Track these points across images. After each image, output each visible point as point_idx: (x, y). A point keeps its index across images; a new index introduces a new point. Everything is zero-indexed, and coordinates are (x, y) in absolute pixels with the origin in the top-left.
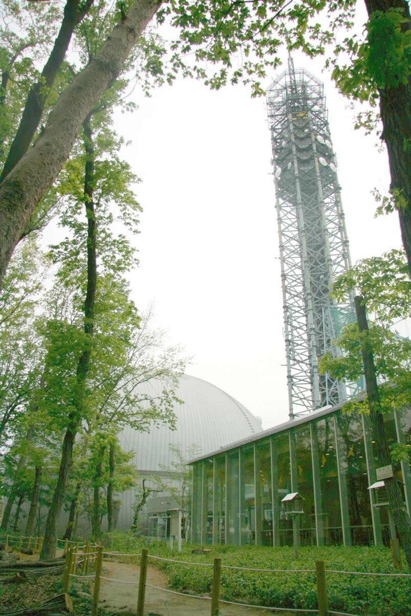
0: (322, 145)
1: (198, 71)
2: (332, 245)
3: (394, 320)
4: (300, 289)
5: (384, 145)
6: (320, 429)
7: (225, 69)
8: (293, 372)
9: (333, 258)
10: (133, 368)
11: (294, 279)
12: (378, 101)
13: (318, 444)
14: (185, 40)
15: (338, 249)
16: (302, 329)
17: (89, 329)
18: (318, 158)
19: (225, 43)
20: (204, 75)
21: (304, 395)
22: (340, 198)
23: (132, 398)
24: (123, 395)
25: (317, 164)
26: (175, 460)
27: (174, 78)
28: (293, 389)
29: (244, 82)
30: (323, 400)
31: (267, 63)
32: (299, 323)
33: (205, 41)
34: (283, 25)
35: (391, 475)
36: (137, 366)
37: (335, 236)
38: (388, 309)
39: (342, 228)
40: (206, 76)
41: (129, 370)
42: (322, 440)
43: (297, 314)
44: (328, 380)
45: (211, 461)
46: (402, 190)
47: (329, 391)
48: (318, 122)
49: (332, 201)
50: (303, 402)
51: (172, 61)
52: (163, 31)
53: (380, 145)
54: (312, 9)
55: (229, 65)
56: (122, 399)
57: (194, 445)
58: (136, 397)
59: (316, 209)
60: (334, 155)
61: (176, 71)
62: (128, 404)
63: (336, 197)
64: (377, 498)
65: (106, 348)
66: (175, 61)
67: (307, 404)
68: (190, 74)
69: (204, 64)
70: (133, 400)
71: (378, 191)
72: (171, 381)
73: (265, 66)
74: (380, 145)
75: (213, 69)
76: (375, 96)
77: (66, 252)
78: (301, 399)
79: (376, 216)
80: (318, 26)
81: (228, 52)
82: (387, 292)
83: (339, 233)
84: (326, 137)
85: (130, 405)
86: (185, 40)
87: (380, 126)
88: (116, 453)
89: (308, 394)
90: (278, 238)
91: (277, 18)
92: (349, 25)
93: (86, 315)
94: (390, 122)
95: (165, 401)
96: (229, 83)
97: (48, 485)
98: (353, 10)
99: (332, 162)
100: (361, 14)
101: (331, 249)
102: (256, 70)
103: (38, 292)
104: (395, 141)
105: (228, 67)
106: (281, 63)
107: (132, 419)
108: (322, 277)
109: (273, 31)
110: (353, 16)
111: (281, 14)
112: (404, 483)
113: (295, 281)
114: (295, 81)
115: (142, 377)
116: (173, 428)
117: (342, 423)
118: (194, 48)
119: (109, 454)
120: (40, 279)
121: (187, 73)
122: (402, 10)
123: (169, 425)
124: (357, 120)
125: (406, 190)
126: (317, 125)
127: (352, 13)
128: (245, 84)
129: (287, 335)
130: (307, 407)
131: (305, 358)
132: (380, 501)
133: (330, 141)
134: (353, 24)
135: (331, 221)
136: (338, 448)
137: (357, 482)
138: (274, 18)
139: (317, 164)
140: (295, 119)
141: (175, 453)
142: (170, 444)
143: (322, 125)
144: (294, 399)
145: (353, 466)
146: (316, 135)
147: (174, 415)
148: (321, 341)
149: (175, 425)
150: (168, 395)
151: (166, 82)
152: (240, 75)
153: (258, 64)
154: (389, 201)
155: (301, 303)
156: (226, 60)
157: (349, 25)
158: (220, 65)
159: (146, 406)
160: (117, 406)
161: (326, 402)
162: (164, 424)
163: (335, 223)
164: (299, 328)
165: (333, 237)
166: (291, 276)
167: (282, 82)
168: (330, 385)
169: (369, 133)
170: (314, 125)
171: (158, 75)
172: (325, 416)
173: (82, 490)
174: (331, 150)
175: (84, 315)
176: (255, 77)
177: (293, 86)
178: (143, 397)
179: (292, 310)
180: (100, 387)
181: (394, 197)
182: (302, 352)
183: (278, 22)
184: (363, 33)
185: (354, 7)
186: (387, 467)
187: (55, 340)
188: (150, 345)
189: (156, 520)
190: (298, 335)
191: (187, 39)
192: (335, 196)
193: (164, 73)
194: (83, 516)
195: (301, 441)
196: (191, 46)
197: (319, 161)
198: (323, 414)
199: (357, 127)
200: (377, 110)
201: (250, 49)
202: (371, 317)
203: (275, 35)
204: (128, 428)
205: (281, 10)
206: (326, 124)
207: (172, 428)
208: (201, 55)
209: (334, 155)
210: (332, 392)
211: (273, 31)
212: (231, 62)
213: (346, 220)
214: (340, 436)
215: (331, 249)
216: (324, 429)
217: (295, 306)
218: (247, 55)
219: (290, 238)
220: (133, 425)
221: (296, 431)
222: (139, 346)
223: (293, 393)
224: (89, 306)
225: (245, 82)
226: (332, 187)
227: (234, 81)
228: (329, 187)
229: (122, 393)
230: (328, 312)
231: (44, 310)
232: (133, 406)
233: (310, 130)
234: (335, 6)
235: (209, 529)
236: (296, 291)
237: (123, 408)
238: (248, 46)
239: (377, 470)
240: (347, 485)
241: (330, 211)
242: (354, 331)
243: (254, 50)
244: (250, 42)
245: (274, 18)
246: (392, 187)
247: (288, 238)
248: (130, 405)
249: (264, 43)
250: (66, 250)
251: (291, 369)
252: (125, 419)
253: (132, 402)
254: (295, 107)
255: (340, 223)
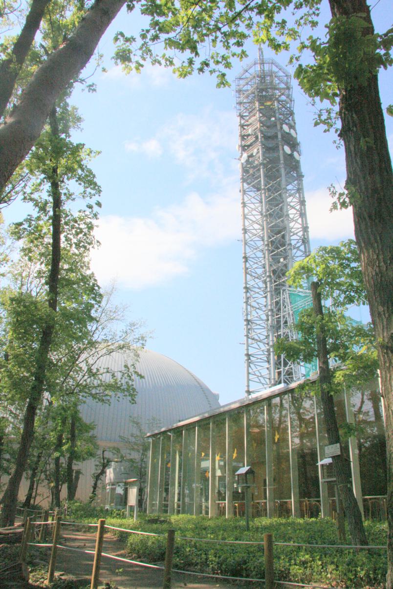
0: (287, 133)
1: (167, 60)
2: (293, 230)
3: (348, 306)
4: (260, 271)
5: (342, 142)
6: (274, 406)
7: (193, 58)
8: (251, 351)
9: (293, 243)
10: (96, 342)
11: (255, 261)
12: (337, 99)
13: (271, 421)
14: (154, 29)
15: (298, 234)
16: (261, 310)
17: (53, 303)
18: (283, 146)
19: (194, 32)
20: (171, 63)
21: (260, 373)
22: (302, 185)
23: (95, 371)
24: (85, 368)
25: (281, 152)
26: (134, 432)
27: (142, 66)
28: (250, 366)
29: (210, 71)
30: (278, 378)
31: (234, 55)
32: (258, 303)
33: (175, 31)
34: (250, 19)
35: (339, 453)
36: (99, 340)
37: (296, 222)
38: (343, 296)
39: (303, 215)
40: (174, 65)
41: (92, 344)
42: (276, 416)
43: (257, 295)
44: (284, 360)
45: (170, 434)
46: (357, 187)
47: (284, 370)
48: (284, 112)
49: (295, 188)
50: (259, 380)
51: (141, 49)
52: (129, 21)
53: (338, 142)
54: (279, 4)
55: (197, 54)
56: (84, 372)
57: (154, 419)
58: (98, 370)
59: (279, 195)
60: (298, 144)
61: (144, 59)
62: (90, 377)
63: (299, 184)
64: (325, 474)
65: (69, 321)
66: (144, 49)
67: (263, 381)
68: (159, 63)
69: (172, 52)
70: (96, 373)
71: (334, 187)
72: (132, 354)
73: (231, 57)
74: (338, 142)
75: (181, 57)
76: (335, 95)
77: (30, 229)
78: (258, 376)
79: (331, 210)
80: (284, 22)
81: (196, 42)
82: (343, 279)
83: (300, 219)
84: (292, 127)
85: (92, 378)
86: (154, 29)
87: (339, 124)
88: (77, 424)
89: (265, 372)
90: (242, 221)
91: (245, 12)
92: (314, 24)
93: (50, 289)
94: (349, 122)
95: (126, 375)
96: (196, 72)
97: (10, 454)
98: (318, 9)
99: (296, 151)
100: (325, 13)
101: (292, 234)
102: (222, 60)
103: (5, 264)
104: (353, 139)
105: (196, 56)
106: (246, 56)
107: (94, 392)
108: (282, 260)
109: (241, 24)
110: (318, 15)
111: (249, 7)
112: (351, 460)
113: (256, 263)
114: (263, 71)
115: (104, 351)
116: (133, 401)
117: (295, 400)
118: (163, 36)
119: (70, 425)
120: (8, 252)
121: (156, 62)
122: (364, 15)
123: (129, 398)
124: (317, 117)
125: (360, 188)
126: (283, 115)
127: (317, 12)
128: (211, 74)
129: (247, 315)
130: (263, 384)
131: (262, 337)
132: (329, 476)
133: (295, 130)
134: (317, 23)
135: (293, 207)
136: (291, 425)
137: (307, 459)
138: (242, 11)
139: (281, 152)
140: (263, 107)
141: (135, 425)
142: (131, 417)
143: (288, 114)
144: (251, 377)
145: (304, 441)
146: (282, 124)
147: (134, 390)
148: (278, 322)
149: (135, 399)
150: (128, 368)
151: (134, 70)
152: (207, 65)
153: (225, 55)
154: (345, 196)
155: (262, 285)
156: (194, 49)
157: (314, 24)
158: (188, 54)
159: (107, 378)
160: (79, 379)
161: (281, 380)
162: (125, 397)
163: (296, 210)
164: (258, 309)
165: (294, 222)
166: (253, 258)
167: (252, 71)
168: (286, 364)
169: (328, 130)
170: (280, 114)
171: (127, 63)
172: (281, 394)
173: (43, 459)
174: (296, 139)
175: (48, 289)
176: (221, 68)
177: (262, 77)
178: (105, 370)
179: (252, 291)
180: (63, 359)
181: (349, 193)
182: (261, 331)
183: (246, 15)
184: (326, 36)
185: (318, 6)
186: (335, 445)
187: (18, 314)
188: (112, 319)
189: (114, 489)
190: (257, 315)
191: (157, 28)
192: (298, 183)
193: (132, 60)
194: (43, 485)
195: (257, 417)
196: (160, 35)
197: (283, 149)
198: (277, 392)
199: (316, 124)
200: (337, 108)
201: (218, 40)
202: (327, 303)
203: (242, 29)
204: (89, 400)
205: (249, 4)
206: (292, 114)
207: (132, 402)
208: (170, 43)
209: (298, 144)
210: (287, 371)
211: (241, 24)
212: (199, 51)
213: (307, 207)
214: (293, 413)
215: (292, 234)
216: (278, 406)
217: (255, 287)
218: (214, 47)
219: (254, 222)
220: (94, 396)
221: (251, 408)
222: (102, 321)
223: (250, 371)
224: (54, 279)
225: (211, 72)
226: (295, 175)
227: (201, 70)
228: (292, 174)
229: (84, 366)
230: (286, 295)
231: (9, 283)
232: (95, 378)
233: (276, 119)
234: (301, 5)
235: (166, 500)
236: (256, 273)
237: (85, 380)
238: (216, 38)
239: (326, 448)
240: (299, 463)
241: (292, 198)
242: (309, 315)
243: (221, 41)
244: (218, 34)
245: (242, 11)
246: (347, 183)
247: (251, 222)
248: (92, 378)
249: (234, 34)
250: (30, 226)
251: (249, 348)
252: (87, 391)
253: (94, 375)
254: (262, 96)
255: (301, 210)
